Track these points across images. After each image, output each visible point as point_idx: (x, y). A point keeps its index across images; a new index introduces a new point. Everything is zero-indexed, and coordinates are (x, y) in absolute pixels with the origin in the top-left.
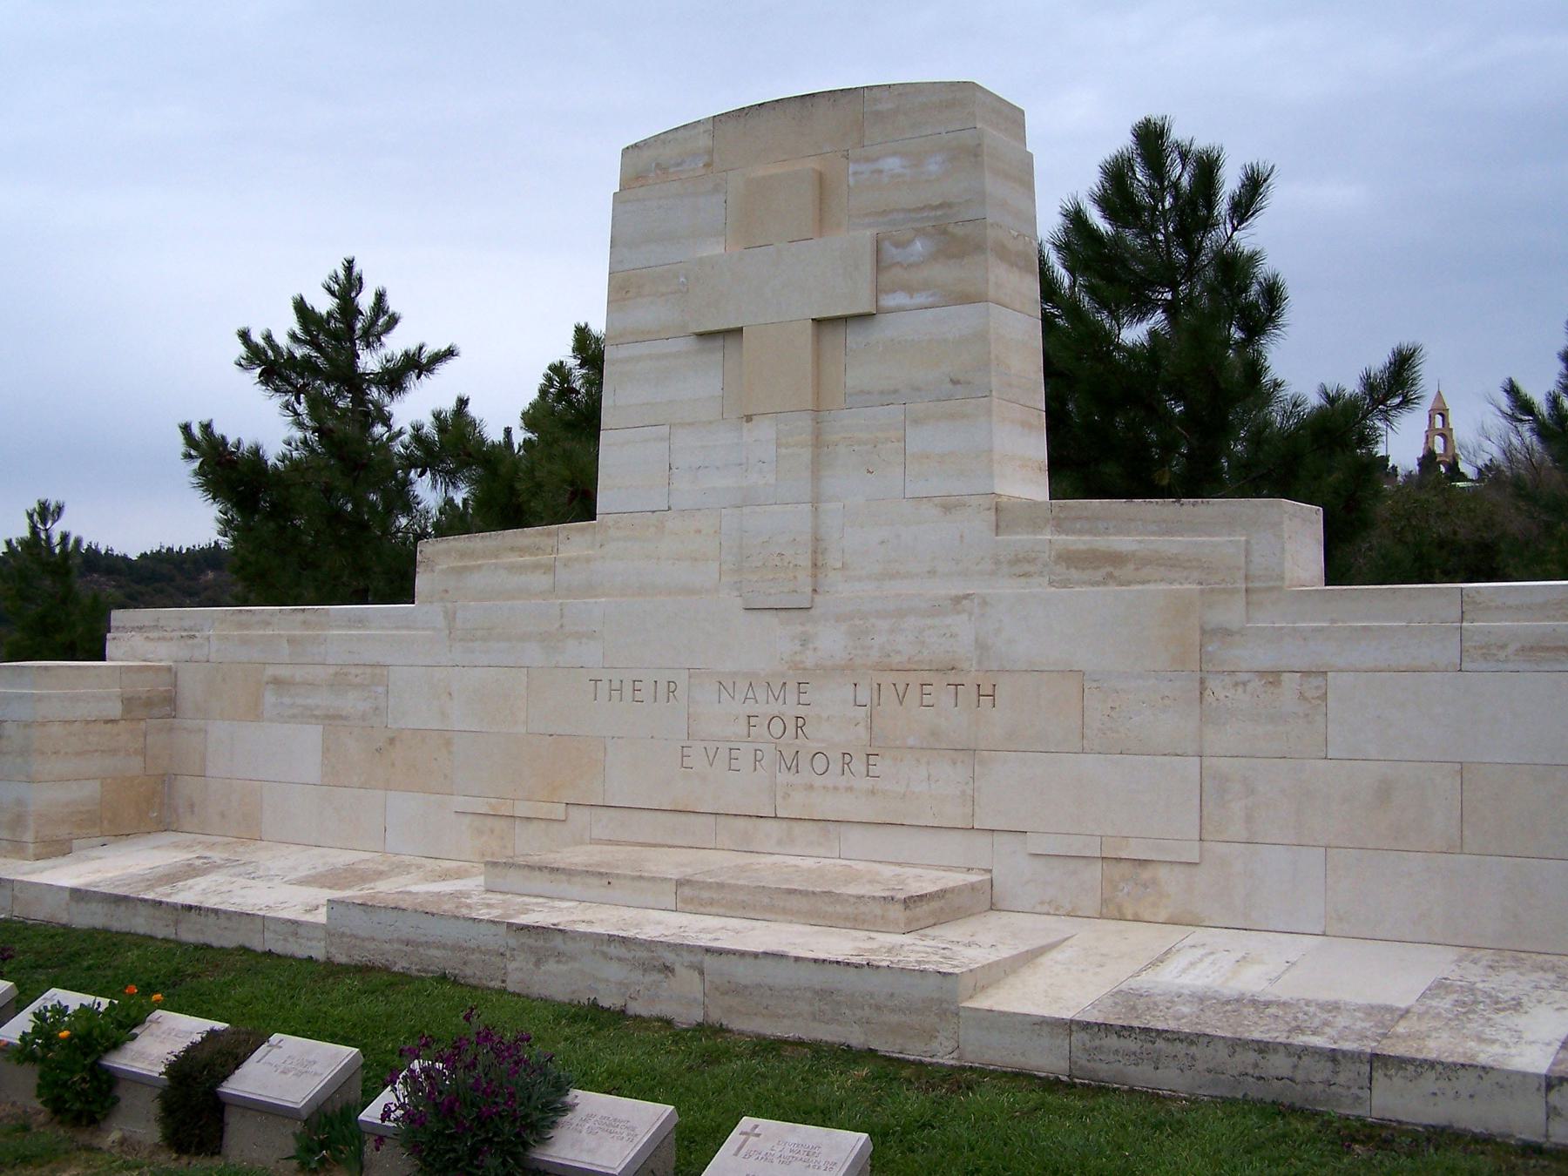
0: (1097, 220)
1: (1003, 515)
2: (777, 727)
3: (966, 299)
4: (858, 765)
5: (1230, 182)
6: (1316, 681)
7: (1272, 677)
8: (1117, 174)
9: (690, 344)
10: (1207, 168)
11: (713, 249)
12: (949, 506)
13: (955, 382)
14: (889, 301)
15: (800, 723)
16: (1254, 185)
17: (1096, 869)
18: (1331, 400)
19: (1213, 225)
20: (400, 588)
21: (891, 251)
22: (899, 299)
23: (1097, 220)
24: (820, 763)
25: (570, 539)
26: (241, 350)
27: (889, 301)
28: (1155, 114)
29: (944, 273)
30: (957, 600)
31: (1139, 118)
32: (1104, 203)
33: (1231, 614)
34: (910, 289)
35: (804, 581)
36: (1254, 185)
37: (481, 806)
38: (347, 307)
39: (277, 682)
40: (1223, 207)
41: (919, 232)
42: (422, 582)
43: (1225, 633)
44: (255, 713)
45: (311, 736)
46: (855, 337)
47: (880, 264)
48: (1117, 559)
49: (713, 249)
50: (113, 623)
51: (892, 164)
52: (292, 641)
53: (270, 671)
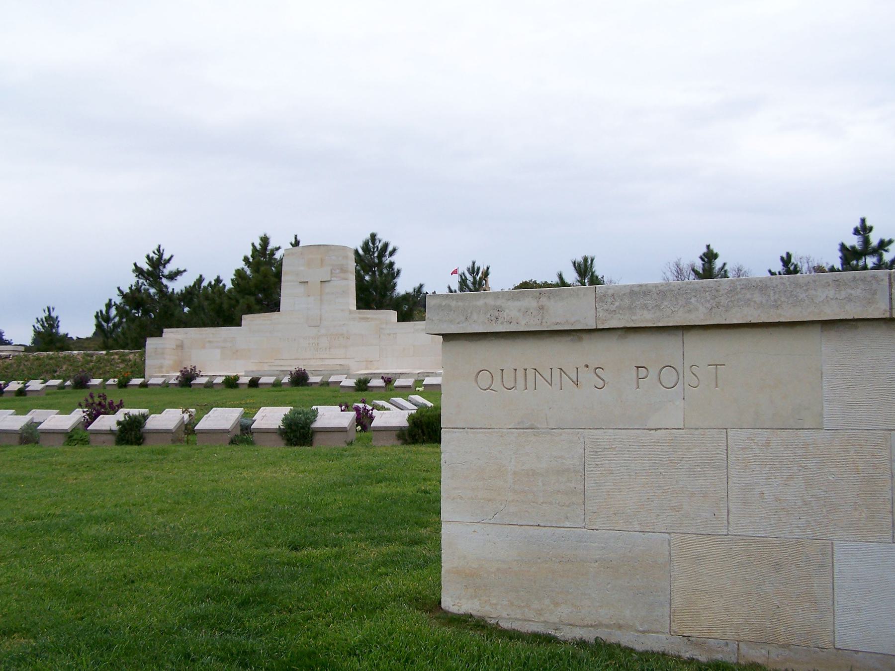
0: (361, 252)
1: (351, 312)
2: (314, 344)
3: (346, 279)
4: (328, 349)
5: (390, 248)
6: (395, 335)
7: (389, 334)
8: (366, 244)
9: (299, 283)
10: (386, 245)
11: (302, 268)
12: (342, 310)
13: (344, 292)
14: (332, 279)
15: (318, 344)
16: (394, 250)
17: (365, 363)
18: (407, 294)
19: (385, 256)
20: (239, 324)
21: (333, 271)
22: (335, 279)
23: (361, 252)
24: (321, 350)
25: (274, 315)
26: (134, 267)
27: (332, 279)
28: (375, 231)
29: (342, 275)
30: (344, 324)
31: (372, 232)
32: (363, 249)
33: (384, 326)
34: (336, 277)
35: (319, 322)
36: (394, 250)
37: (256, 361)
38: (161, 255)
39: (210, 342)
40: (387, 253)
41: (338, 269)
42: (243, 322)
43: (383, 329)
44: (204, 347)
45: (218, 351)
46: (327, 284)
47: (331, 273)
48: (368, 318)
49: (302, 268)
50: (164, 331)
51: (333, 258)
52: (213, 334)
53: (207, 340)
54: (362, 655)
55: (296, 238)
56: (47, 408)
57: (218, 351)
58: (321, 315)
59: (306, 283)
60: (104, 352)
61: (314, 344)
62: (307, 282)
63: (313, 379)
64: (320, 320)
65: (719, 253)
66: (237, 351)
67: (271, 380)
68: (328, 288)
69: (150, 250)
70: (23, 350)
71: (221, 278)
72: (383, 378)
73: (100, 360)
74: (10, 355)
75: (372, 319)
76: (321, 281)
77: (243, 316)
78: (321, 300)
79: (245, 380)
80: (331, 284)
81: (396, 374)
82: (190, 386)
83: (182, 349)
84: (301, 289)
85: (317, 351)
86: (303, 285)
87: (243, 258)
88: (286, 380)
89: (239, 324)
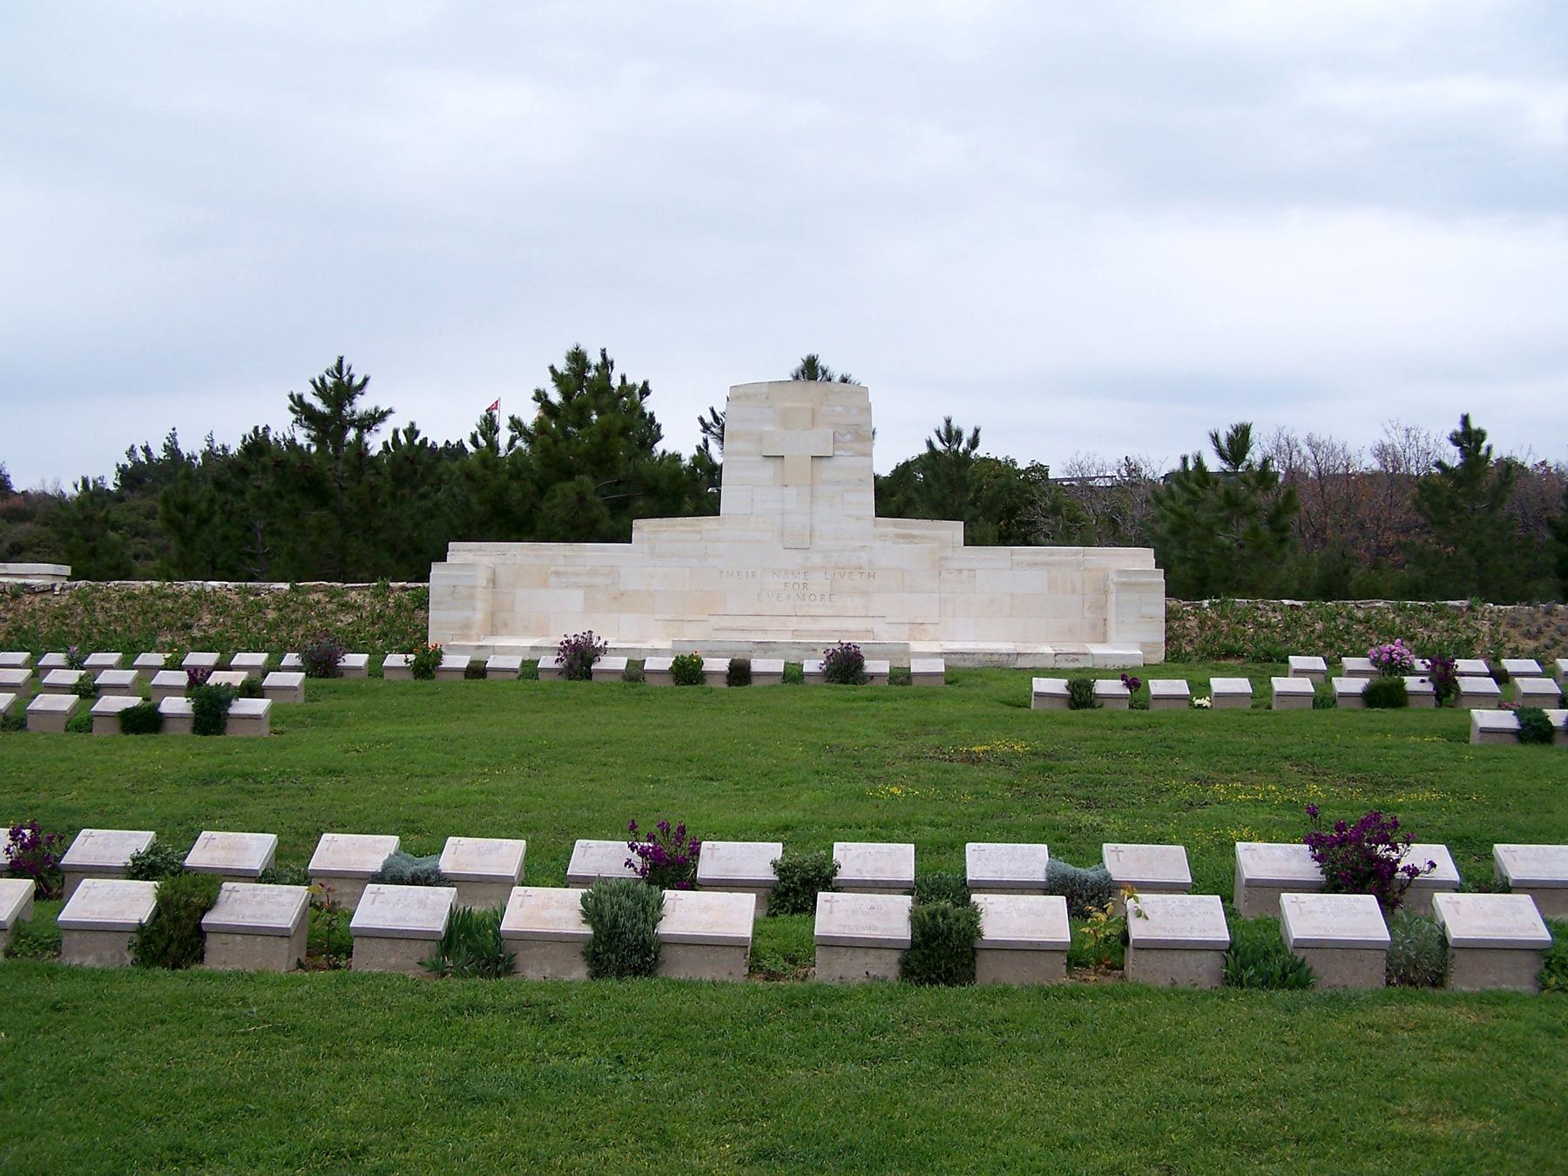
4: (827, 598)
7: (960, 570)
11: (769, 428)
14: (837, 453)
21: (839, 438)
22: (842, 452)
27: (837, 453)
29: (857, 446)
35: (807, 539)
39: (557, 573)
44: (544, 584)
45: (578, 595)
46: (824, 462)
48: (914, 537)
49: (769, 428)
53: (552, 569)
54: (545, 1057)
55: (604, 356)
56: (874, 838)
57: (578, 595)
58: (811, 527)
59: (778, 461)
60: (286, 586)
61: (796, 587)
62: (783, 457)
63: (872, 666)
64: (811, 536)
65: (1483, 427)
66: (622, 594)
67: (777, 666)
68: (827, 471)
69: (321, 366)
70: (69, 573)
71: (417, 428)
72: (1123, 678)
73: (282, 603)
74: (53, 586)
75: (923, 538)
76: (812, 457)
77: (634, 521)
78: (812, 496)
79: (717, 664)
80: (834, 462)
81: (1008, 654)
82: (589, 675)
83: (494, 588)
84: (768, 471)
85: (804, 599)
86: (770, 464)
87: (533, 394)
88: (812, 665)
89: (627, 538)
